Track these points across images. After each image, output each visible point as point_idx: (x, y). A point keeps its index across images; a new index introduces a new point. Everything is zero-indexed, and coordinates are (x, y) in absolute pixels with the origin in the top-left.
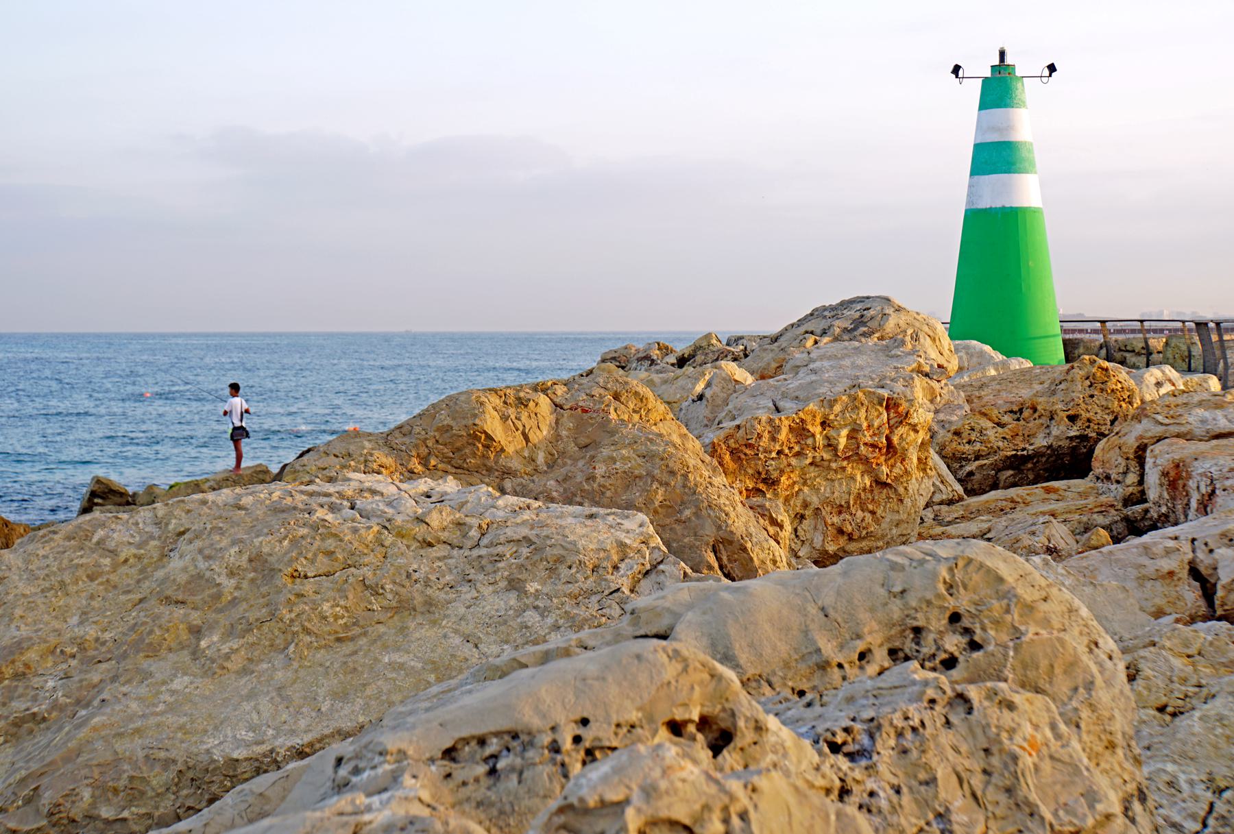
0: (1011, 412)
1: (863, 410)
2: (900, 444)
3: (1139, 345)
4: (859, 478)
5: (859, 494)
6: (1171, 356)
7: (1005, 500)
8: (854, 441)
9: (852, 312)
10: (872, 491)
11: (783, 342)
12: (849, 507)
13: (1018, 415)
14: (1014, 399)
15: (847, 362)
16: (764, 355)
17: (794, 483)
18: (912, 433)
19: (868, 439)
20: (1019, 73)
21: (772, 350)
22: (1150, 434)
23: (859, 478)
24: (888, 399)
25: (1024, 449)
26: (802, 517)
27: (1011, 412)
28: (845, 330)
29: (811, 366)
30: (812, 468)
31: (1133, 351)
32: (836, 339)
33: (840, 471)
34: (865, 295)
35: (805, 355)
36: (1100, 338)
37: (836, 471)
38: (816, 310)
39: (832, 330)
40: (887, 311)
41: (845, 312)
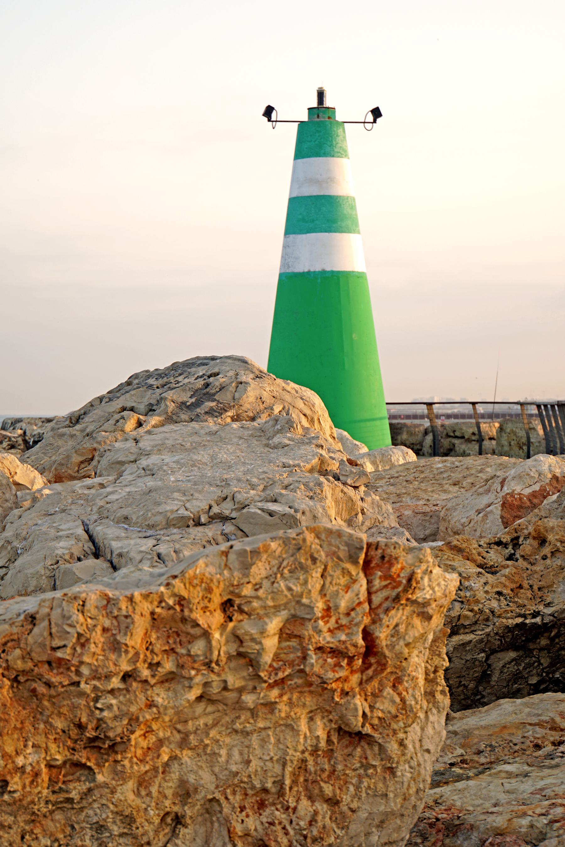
0: (499, 543)
1: (316, 573)
2: (392, 647)
3: (469, 431)
4: (303, 726)
5: (304, 761)
6: (506, 443)
7: (539, 724)
8: (294, 643)
9: (192, 380)
10: (330, 753)
11: (88, 424)
12: (281, 793)
13: (510, 550)
14: (427, 509)
15: (203, 456)
16: (60, 443)
17: (161, 742)
18: (417, 621)
19: (326, 639)
20: (339, 117)
21: (72, 436)
23: (303, 726)
24: (369, 545)
25: (535, 614)
26: (178, 820)
27: (499, 543)
28: (183, 405)
29: (144, 462)
30: (200, 708)
31: (463, 437)
32: (171, 419)
33: (262, 711)
34: (209, 355)
35: (130, 444)
36: (427, 423)
37: (253, 713)
38: (136, 376)
39: (163, 405)
40: (243, 378)
41: (180, 378)
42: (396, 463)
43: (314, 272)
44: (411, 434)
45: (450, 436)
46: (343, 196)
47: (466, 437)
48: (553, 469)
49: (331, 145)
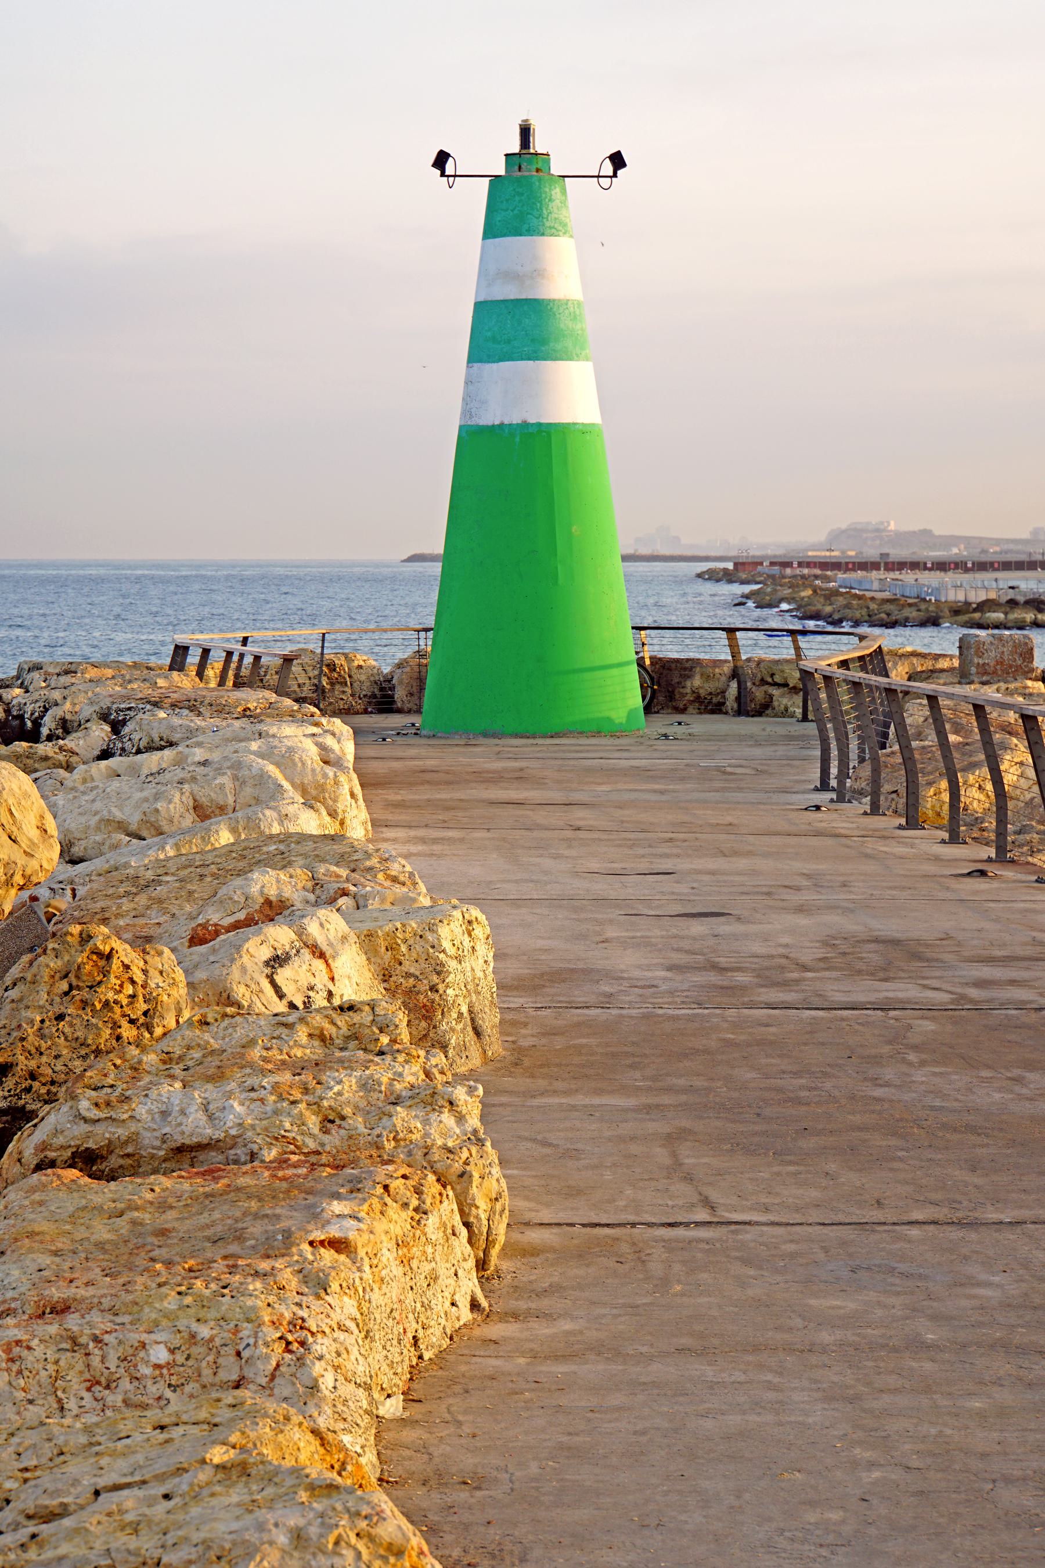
20: (556, 170)
22: (60, 1140)
31: (786, 685)
42: (267, 832)
43: (510, 425)
44: (707, 678)
45: (768, 683)
46: (559, 300)
47: (791, 685)
48: (266, 890)
49: (540, 216)
